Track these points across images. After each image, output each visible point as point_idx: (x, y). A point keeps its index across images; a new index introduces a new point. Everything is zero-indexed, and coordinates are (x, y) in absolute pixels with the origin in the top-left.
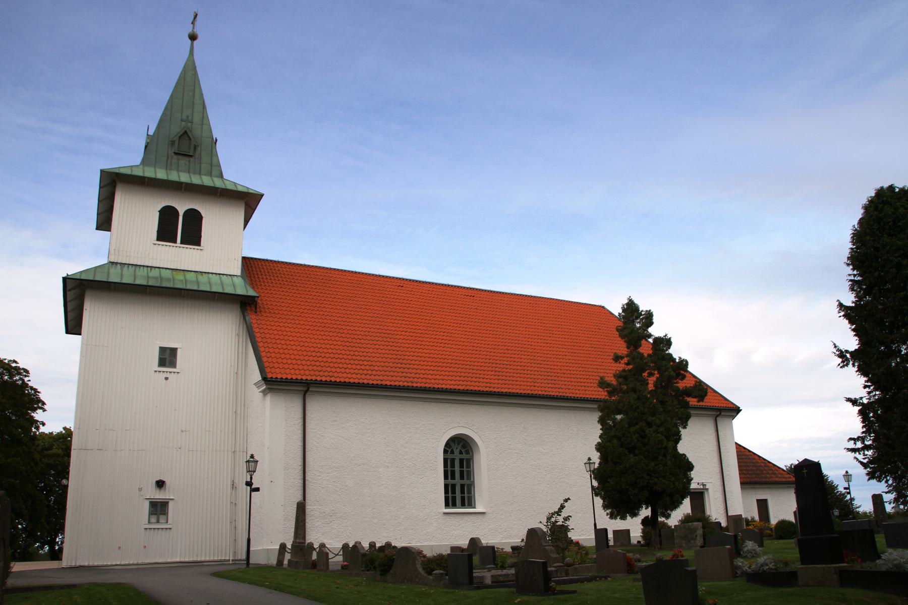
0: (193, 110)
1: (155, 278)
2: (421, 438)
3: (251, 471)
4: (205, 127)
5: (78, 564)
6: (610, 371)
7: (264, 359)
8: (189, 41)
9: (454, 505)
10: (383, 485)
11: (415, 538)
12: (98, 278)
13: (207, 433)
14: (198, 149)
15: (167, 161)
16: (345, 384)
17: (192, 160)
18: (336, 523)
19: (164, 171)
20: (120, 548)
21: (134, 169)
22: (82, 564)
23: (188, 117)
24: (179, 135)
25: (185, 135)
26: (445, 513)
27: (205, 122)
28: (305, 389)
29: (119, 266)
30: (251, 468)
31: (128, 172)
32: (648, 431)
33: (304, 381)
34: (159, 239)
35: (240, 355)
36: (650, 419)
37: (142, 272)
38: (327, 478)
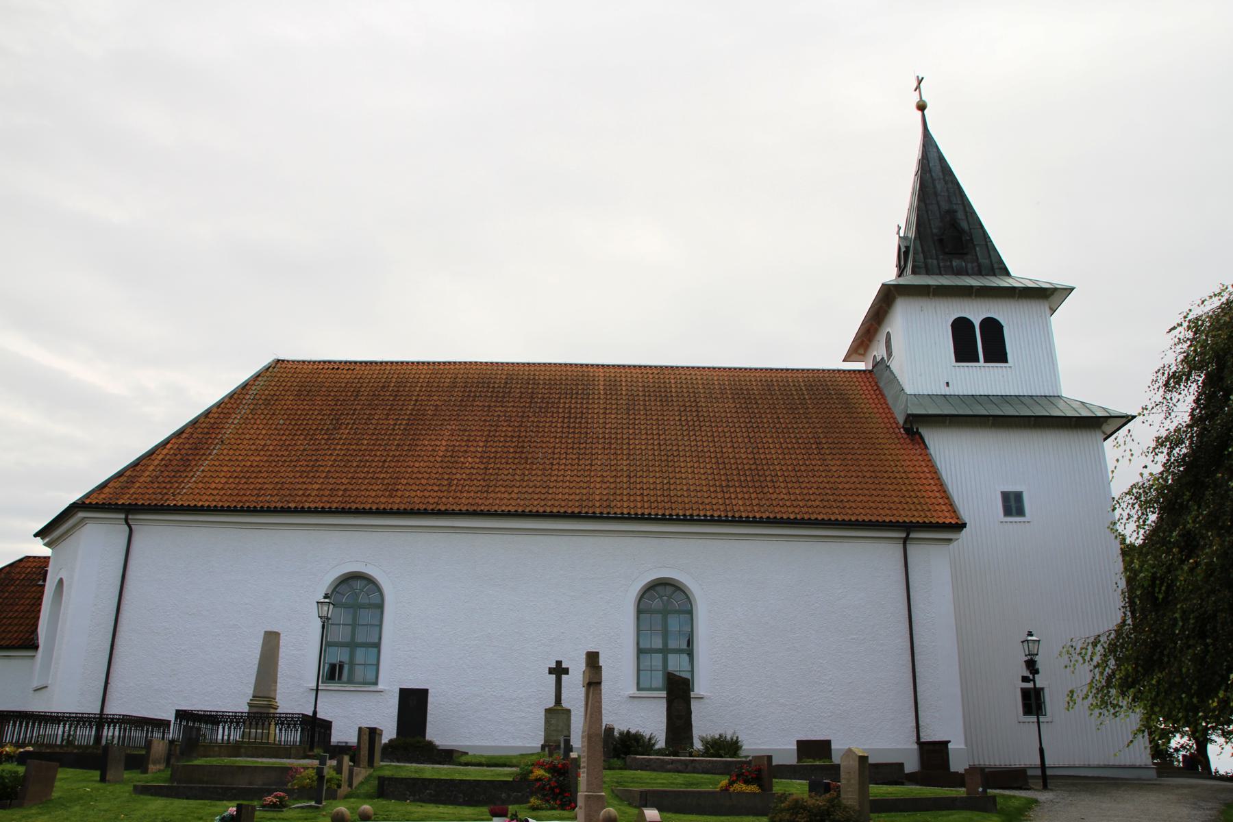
8: (920, 113)
16: (885, 524)
34: (957, 360)
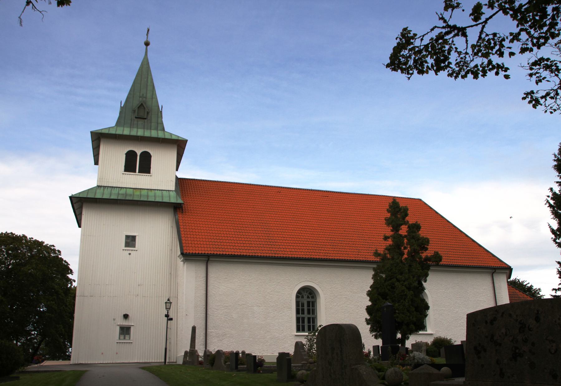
0: (147, 89)
1: (123, 194)
2: (281, 288)
3: (168, 309)
4: (154, 100)
5: (79, 362)
6: (382, 246)
7: (184, 242)
8: (145, 46)
9: (303, 330)
10: (256, 317)
11: (276, 350)
12: (89, 196)
13: (154, 286)
14: (149, 116)
15: (131, 122)
17: (146, 120)
18: (225, 340)
19: (129, 129)
20: (102, 353)
21: (111, 129)
22: (81, 362)
23: (143, 95)
24: (138, 106)
25: (141, 106)
26: (296, 335)
27: (154, 96)
28: (207, 259)
29: (102, 188)
30: (168, 306)
31: (107, 132)
32: (397, 284)
33: (206, 255)
35: (174, 239)
36: (399, 277)
37: (115, 191)
38: (221, 313)
